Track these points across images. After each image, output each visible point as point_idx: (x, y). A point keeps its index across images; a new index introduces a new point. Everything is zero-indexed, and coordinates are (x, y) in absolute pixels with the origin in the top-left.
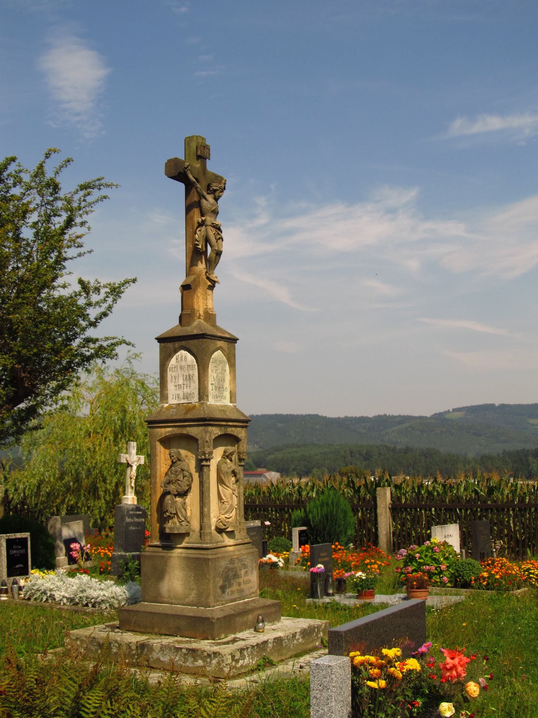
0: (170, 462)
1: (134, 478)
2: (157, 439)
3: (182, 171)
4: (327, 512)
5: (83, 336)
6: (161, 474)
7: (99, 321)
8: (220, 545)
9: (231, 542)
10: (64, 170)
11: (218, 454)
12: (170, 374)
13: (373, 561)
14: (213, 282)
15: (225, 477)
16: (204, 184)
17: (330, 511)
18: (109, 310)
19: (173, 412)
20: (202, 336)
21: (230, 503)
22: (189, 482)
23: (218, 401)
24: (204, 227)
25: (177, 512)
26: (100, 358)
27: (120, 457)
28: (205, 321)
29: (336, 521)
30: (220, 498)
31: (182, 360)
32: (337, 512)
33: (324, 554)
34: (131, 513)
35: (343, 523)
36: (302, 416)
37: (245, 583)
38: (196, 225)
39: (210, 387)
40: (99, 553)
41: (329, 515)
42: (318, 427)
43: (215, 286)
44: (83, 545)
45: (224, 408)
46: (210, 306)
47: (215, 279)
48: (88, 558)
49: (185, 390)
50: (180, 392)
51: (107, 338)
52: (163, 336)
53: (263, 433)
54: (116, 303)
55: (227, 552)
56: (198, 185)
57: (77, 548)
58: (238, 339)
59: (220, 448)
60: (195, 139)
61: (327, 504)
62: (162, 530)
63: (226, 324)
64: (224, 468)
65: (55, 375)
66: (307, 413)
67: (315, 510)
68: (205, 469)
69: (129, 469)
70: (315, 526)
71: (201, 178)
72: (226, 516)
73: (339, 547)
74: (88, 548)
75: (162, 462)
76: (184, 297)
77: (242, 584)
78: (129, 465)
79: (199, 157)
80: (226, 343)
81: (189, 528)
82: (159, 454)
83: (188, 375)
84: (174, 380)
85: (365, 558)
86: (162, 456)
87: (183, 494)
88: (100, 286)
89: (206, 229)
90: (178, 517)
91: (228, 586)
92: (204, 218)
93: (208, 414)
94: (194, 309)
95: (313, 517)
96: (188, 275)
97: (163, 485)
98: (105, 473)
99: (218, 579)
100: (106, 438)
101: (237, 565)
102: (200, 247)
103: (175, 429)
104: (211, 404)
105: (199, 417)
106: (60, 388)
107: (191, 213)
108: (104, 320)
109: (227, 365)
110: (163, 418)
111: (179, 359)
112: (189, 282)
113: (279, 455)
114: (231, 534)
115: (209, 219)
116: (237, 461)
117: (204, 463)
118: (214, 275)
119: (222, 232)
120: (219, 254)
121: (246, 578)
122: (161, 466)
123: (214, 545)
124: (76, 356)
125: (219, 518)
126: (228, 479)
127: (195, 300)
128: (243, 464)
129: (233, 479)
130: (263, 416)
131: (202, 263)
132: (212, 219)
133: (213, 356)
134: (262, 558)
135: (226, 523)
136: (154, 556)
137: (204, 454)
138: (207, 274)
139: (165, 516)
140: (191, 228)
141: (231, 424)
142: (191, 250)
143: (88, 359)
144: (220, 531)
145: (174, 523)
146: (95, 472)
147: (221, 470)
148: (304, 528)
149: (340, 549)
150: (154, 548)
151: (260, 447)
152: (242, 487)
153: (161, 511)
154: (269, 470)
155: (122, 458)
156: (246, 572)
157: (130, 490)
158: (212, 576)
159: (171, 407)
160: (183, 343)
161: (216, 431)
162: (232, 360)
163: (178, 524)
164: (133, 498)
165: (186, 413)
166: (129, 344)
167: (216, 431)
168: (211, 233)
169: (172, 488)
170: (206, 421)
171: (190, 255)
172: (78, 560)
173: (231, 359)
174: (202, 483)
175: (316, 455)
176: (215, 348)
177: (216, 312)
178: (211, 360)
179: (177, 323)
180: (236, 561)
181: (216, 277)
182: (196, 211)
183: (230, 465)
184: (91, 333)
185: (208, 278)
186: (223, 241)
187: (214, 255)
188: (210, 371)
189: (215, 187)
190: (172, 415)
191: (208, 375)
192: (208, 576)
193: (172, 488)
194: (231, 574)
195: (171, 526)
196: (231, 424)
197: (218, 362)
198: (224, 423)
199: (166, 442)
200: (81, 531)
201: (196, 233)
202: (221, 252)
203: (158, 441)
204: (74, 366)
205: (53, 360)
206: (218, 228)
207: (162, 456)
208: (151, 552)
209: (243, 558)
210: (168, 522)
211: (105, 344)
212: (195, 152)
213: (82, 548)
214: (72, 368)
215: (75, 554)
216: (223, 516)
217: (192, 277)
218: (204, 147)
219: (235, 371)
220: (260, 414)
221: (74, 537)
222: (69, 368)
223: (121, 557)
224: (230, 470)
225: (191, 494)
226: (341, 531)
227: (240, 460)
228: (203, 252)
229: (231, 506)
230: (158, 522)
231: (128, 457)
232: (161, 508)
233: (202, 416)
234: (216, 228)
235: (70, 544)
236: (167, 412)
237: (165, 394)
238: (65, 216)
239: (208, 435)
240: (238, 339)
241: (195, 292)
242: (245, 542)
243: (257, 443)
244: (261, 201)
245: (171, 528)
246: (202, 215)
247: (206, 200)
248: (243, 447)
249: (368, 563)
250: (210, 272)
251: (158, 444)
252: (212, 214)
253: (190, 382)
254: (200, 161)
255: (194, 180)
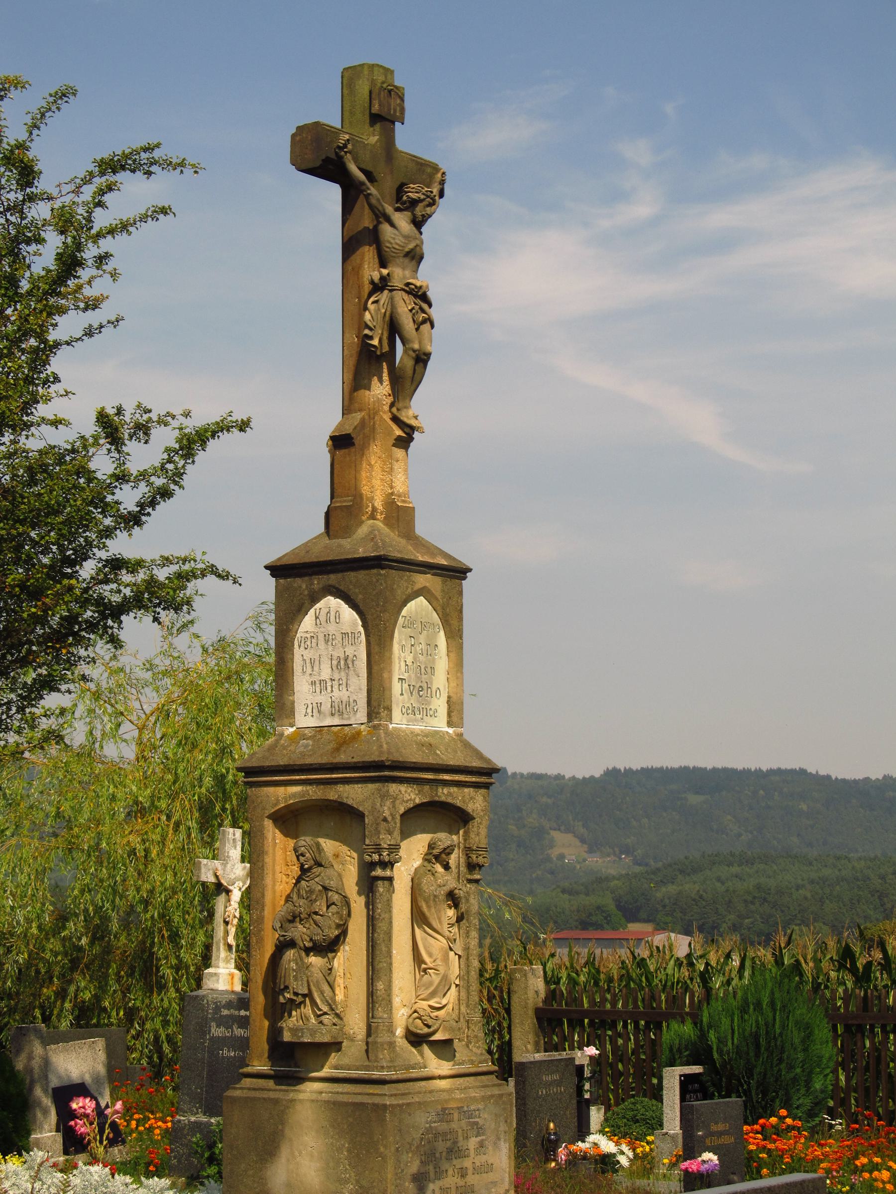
0: (296, 870)
1: (235, 921)
2: (267, 813)
3: (333, 156)
4: (758, 1027)
5: (103, 554)
6: (274, 898)
7: (150, 510)
8: (414, 1073)
9: (443, 1067)
10: (54, 120)
11: (413, 852)
12: (300, 655)
13: (877, 1160)
14: (407, 430)
15: (429, 907)
16: (389, 184)
17: (766, 1024)
18: (176, 483)
19: (306, 746)
20: (378, 562)
21: (442, 970)
22: (341, 919)
23: (416, 720)
24: (386, 292)
25: (309, 990)
26: (146, 608)
27: (198, 866)
28: (386, 525)
29: (782, 1051)
30: (418, 959)
31: (328, 620)
32: (784, 1027)
33: (721, 1127)
34: (225, 1012)
35: (801, 1056)
36: (758, 772)
37: (477, 1170)
38: (367, 288)
39: (396, 687)
40: (150, 1129)
41: (763, 1032)
42: (804, 807)
43: (412, 439)
44: (103, 1105)
45: (428, 742)
46: (399, 487)
47: (413, 422)
48: (117, 1138)
49: (336, 693)
50: (324, 699)
51: (167, 559)
52: (285, 562)
53: (645, 820)
54: (193, 462)
55: (431, 1092)
56: (373, 190)
57: (89, 1111)
58: (470, 570)
59: (419, 836)
60: (366, 72)
61: (758, 1005)
62: (275, 1033)
63: (439, 531)
64: (429, 885)
65: (30, 651)
66: (775, 766)
67: (725, 1022)
68: (381, 887)
69: (222, 898)
70: (724, 1064)
71: (381, 171)
72: (432, 1003)
73: (789, 1121)
74: (117, 1112)
75: (278, 869)
76: (336, 466)
77: (470, 1172)
78: (220, 888)
79: (375, 118)
80: (438, 580)
81: (341, 1030)
82: (271, 851)
83: (342, 656)
84: (309, 671)
85: (857, 1153)
86: (279, 853)
87: (328, 947)
88: (150, 420)
89: (392, 299)
90: (314, 1003)
91: (432, 1175)
92: (385, 272)
93: (389, 753)
94: (361, 496)
95: (719, 1040)
96: (347, 410)
97: (278, 925)
98: (176, 919)
99: (406, 1157)
100: (177, 825)
101: (458, 1124)
102: (375, 342)
103: (309, 788)
104: (400, 729)
105: (367, 759)
106: (43, 687)
107: (355, 258)
108: (163, 507)
109: (442, 633)
110: (282, 761)
111: (322, 618)
112: (348, 429)
113: (690, 887)
114: (444, 1048)
115: (399, 274)
116: (463, 869)
117: (379, 872)
118: (411, 413)
119: (430, 306)
120: (422, 359)
121: (480, 1160)
122: (274, 881)
123: (401, 1075)
124: (84, 603)
125: (416, 1007)
126: (438, 911)
127: (364, 474)
128: (477, 877)
129: (451, 913)
130: (647, 772)
131: (381, 381)
132: (407, 273)
133: (404, 612)
134: (573, 1142)
135: (430, 1022)
136: (254, 1099)
137: (378, 849)
138: (394, 410)
139: (282, 1000)
140: (356, 294)
141: (446, 777)
142: (355, 349)
143: (117, 612)
144: (416, 1039)
145: (304, 1018)
146: (148, 916)
147: (420, 889)
148: (697, 1069)
149: (790, 1128)
150: (254, 1080)
151: (637, 863)
152: (474, 934)
153: (273, 989)
154: (661, 927)
155: (203, 870)
156: (481, 1145)
157: (223, 953)
158: (393, 1149)
159: (300, 734)
160: (333, 579)
161: (409, 795)
162: (454, 622)
163: (313, 1020)
164: (232, 976)
165: (337, 750)
166: (223, 576)
167: (409, 795)
168: (404, 306)
169: (299, 932)
170: (383, 771)
171: (352, 362)
172: (89, 1142)
173: (452, 619)
174: (371, 921)
175: (798, 887)
176: (409, 590)
177: (415, 501)
178: (401, 620)
179: (321, 528)
180: (456, 1116)
181: (416, 417)
182: (368, 254)
183: (444, 879)
184: (122, 545)
185: (396, 419)
186: (432, 326)
187: (410, 363)
188: (396, 647)
189: (417, 190)
190: (303, 755)
191: (390, 658)
192: (382, 1149)
193: (299, 932)
194: (441, 1146)
195: (299, 1025)
196: (446, 777)
197: (417, 625)
198: (430, 776)
199: (289, 820)
200: (102, 1070)
201: (366, 308)
202: (428, 355)
203: (269, 817)
204: (80, 630)
205: (25, 615)
206: (421, 296)
207: (279, 853)
208: (249, 1089)
209: (472, 1108)
210: (290, 1016)
211: (162, 574)
212: (367, 105)
213: (100, 1112)
214: (75, 635)
215: (81, 1127)
216: (424, 1004)
217: (358, 416)
218: (390, 91)
219: (460, 647)
220: (636, 765)
221: (80, 1081)
222: (69, 633)
223: (197, 1127)
224: (443, 891)
225: (347, 948)
226: (795, 1080)
227: (472, 867)
228: (383, 355)
229: (445, 978)
230: (266, 1016)
231: (220, 868)
232: (275, 983)
233: (375, 757)
234: (416, 296)
235: (71, 1100)
236: (292, 748)
237: (288, 704)
238: (54, 242)
239: (388, 803)
240: (470, 570)
241: (363, 454)
242: (480, 1070)
243: (627, 850)
244: (638, 151)
245: (294, 1031)
246: (383, 264)
247: (392, 225)
248: (478, 834)
249: (863, 1165)
250: (400, 405)
251: (268, 824)
252: (407, 260)
253: (347, 675)
254: (378, 127)
255: (361, 176)
